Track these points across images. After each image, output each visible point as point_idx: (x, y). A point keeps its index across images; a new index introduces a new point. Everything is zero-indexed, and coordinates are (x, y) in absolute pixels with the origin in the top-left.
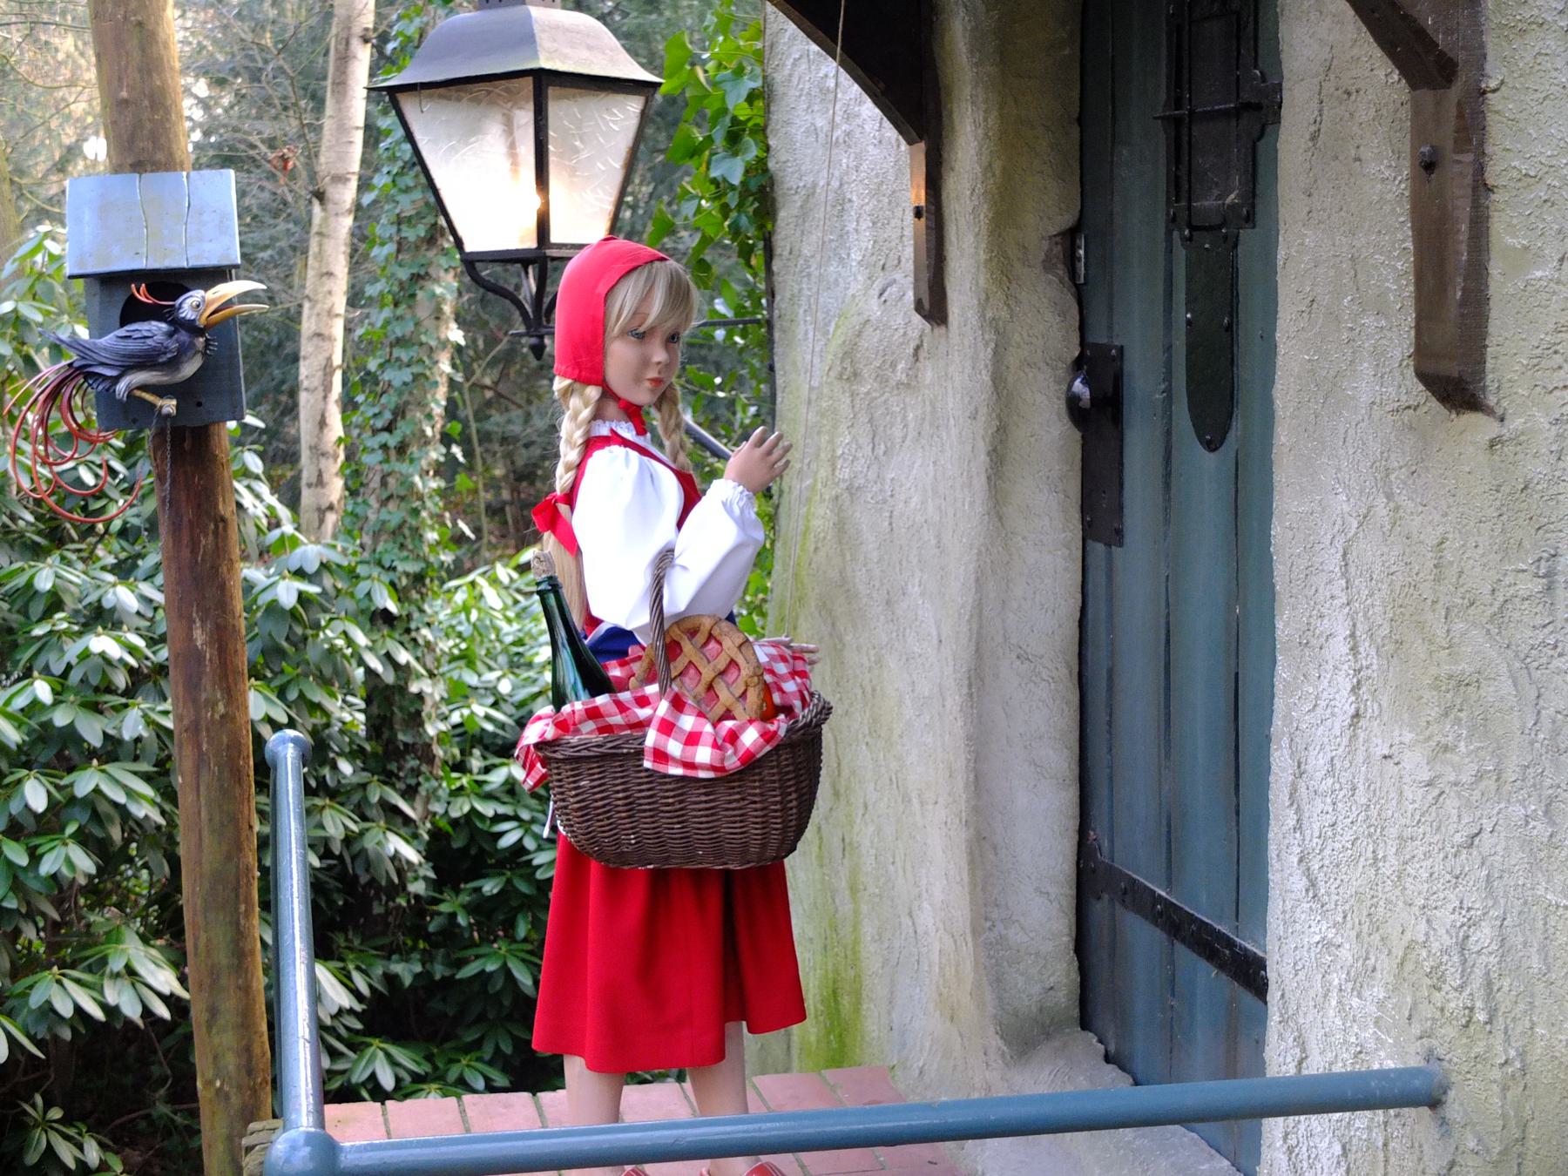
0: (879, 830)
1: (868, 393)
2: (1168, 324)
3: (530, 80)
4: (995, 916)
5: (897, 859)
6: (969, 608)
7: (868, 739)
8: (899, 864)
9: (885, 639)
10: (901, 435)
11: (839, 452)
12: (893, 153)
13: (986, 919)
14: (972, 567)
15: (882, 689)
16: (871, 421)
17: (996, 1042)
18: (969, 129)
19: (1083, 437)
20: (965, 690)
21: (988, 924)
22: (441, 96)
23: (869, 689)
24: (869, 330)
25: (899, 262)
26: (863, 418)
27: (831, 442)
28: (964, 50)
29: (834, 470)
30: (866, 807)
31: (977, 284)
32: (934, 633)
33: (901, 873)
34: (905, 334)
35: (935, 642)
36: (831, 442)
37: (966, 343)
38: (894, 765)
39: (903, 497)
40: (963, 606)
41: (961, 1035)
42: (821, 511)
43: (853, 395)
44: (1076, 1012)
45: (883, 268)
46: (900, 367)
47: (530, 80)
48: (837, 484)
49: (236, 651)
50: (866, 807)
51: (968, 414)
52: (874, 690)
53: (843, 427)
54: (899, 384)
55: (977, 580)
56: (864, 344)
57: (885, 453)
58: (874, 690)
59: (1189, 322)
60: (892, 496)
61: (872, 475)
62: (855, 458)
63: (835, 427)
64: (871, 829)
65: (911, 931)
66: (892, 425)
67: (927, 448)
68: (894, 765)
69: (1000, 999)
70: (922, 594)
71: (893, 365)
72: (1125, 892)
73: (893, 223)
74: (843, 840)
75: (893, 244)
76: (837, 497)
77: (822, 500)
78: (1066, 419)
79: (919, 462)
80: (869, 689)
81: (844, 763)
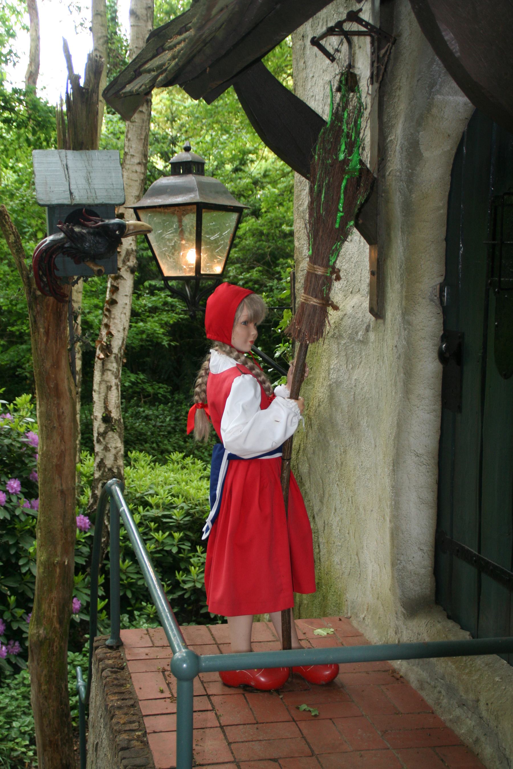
0: (342, 520)
1: (345, 344)
2: (486, 327)
3: (195, 206)
4: (402, 559)
5: (351, 532)
6: (394, 434)
7: (338, 482)
8: (351, 534)
9: (348, 443)
10: (359, 361)
11: (332, 367)
12: (357, 246)
13: (398, 560)
14: (395, 418)
15: (346, 463)
16: (346, 355)
17: (401, 609)
18: (399, 241)
19: (444, 368)
20: (391, 468)
21: (399, 562)
22: (160, 212)
23: (339, 462)
24: (346, 318)
25: (359, 290)
26: (343, 353)
27: (328, 362)
28: (399, 210)
29: (329, 374)
30: (335, 510)
31: (401, 304)
32: (373, 442)
33: (352, 537)
34: (362, 321)
35: (373, 446)
36: (328, 362)
37: (395, 327)
38: (351, 494)
39: (360, 386)
40: (391, 434)
41: (383, 605)
42: (322, 390)
43: (339, 344)
44: (433, 598)
45: (351, 293)
46: (360, 334)
47: (195, 206)
48: (330, 380)
49: (306, 493)
50: (335, 510)
51: (396, 357)
52: (342, 463)
53: (334, 357)
54: (360, 341)
55: (398, 424)
56: (343, 323)
57: (352, 368)
58: (342, 463)
59: (497, 326)
60: (355, 386)
61: (346, 377)
62: (339, 370)
63: (330, 356)
64: (338, 519)
65: (357, 561)
66: (355, 357)
67: (372, 367)
68: (351, 494)
69: (403, 592)
70: (368, 426)
71: (357, 333)
72: (458, 551)
73: (356, 274)
74: (324, 523)
75: (356, 283)
76: (330, 385)
77: (323, 386)
78: (438, 360)
79: (367, 373)
80: (339, 462)
81: (326, 492)
